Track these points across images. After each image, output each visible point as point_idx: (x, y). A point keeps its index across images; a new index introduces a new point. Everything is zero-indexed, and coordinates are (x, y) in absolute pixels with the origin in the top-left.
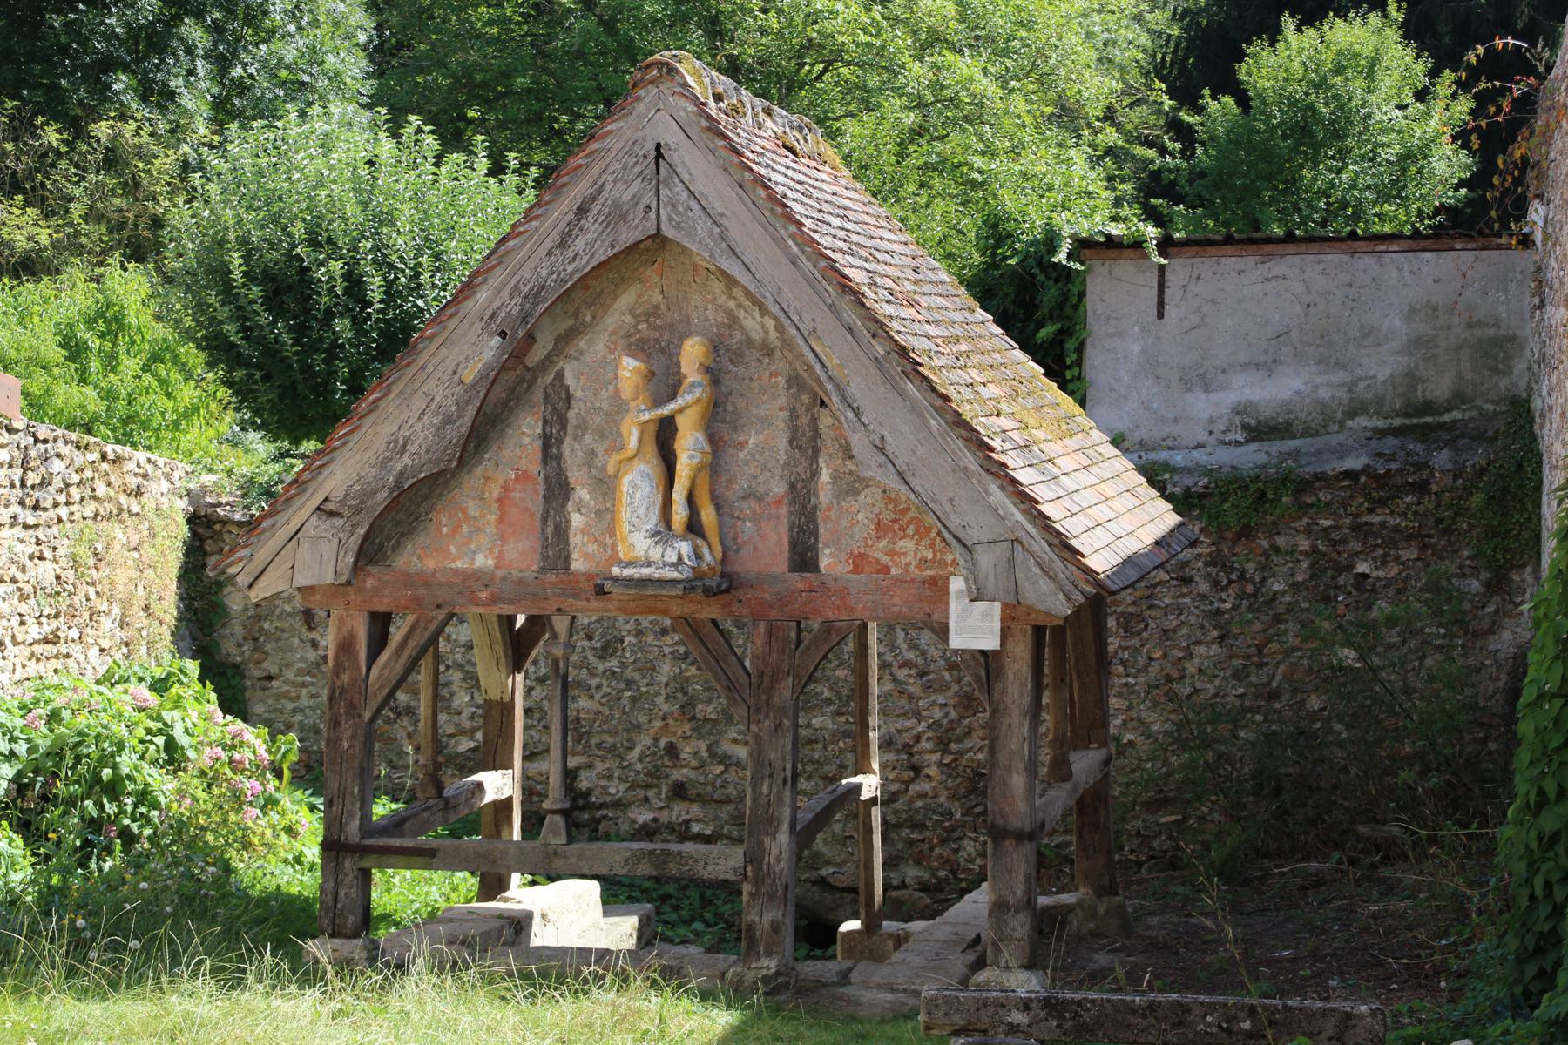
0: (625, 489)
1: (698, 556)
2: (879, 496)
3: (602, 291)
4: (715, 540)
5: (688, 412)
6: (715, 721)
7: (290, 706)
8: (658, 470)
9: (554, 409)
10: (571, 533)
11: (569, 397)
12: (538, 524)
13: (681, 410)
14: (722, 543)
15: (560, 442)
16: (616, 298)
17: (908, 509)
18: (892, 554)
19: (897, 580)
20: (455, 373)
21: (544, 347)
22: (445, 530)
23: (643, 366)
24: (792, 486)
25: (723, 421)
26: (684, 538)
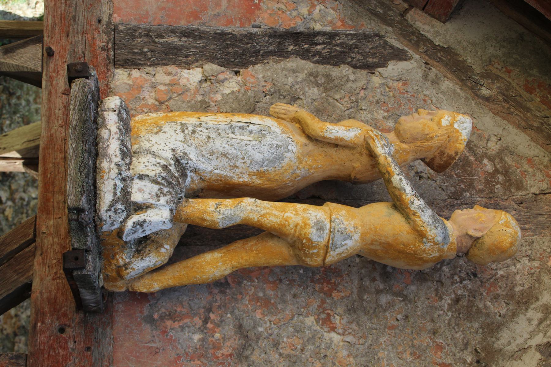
3: (528, 110)
5: (397, 219)
6: (12, 349)
7: (31, 99)
8: (288, 177)
10: (171, 69)
11: (371, 68)
12: (183, 24)
14: (167, 292)
15: (305, 55)
25: (362, 289)
26: (175, 218)
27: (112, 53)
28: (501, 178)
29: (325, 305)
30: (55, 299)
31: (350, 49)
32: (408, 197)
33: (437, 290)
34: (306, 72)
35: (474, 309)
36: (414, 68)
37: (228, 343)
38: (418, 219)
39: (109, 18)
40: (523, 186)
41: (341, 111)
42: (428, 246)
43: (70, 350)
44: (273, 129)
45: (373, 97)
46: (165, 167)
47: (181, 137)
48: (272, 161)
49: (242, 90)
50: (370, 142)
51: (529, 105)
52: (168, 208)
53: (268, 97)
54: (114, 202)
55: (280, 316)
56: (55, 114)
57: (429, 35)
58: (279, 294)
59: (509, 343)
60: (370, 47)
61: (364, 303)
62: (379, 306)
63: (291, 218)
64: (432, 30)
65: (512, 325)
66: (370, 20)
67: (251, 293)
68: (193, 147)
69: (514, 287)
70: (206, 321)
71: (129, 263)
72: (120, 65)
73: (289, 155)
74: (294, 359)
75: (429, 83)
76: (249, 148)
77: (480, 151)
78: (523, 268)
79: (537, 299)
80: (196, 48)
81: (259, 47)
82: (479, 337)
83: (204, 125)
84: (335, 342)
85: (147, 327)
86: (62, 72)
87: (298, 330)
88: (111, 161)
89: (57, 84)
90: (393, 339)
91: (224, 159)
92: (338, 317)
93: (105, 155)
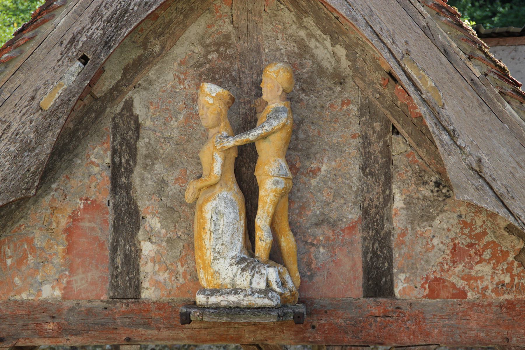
0: (208, 216)
1: (283, 284)
2: (455, 222)
3: (171, 22)
4: (294, 267)
5: (272, 138)
9: (124, 139)
10: (142, 262)
11: (138, 127)
12: (108, 253)
13: (265, 137)
15: (130, 171)
16: (185, 28)
17: (485, 233)
18: (468, 278)
19: (474, 305)
20: (33, 98)
21: (112, 77)
22: (9, 262)
23: (226, 92)
24: (366, 212)
27: (130, 300)
28: (222, 49)
29: (305, 172)
30: (295, 331)
31: (124, 139)
32: (263, 132)
33: (297, 102)
34: (143, 171)
35: (309, 80)
36: (140, 96)
37: (326, 232)
38: (276, 128)
39: (104, 302)
40: (227, 35)
41: (172, 150)
42: (289, 121)
43: (326, 322)
44: (214, 206)
45: (161, 127)
46: (243, 270)
47: (222, 260)
48: (233, 206)
49: (159, 215)
50: (225, 149)
51: (167, 19)
52: (268, 269)
53: (162, 199)
54: (268, 298)
55: (311, 201)
56: (173, 336)
57: (114, 83)
58: (297, 200)
59: (330, 62)
60: (122, 125)
61: (304, 148)
62: (306, 139)
63: (271, 199)
64: (109, 80)
65: (319, 59)
66: (102, 123)
67: (296, 217)
68: (229, 254)
69: (295, 53)
70: (312, 244)
71: (290, 290)
72: (139, 295)
73: (229, 196)
74: (336, 194)
75: (150, 87)
76: (228, 221)
77: (202, 60)
78: (282, 44)
79: (303, 39)
80: (125, 245)
81: (124, 202)
82: (326, 80)
83: (214, 247)
84: (327, 168)
85: (315, 279)
86: (143, 332)
87: (319, 190)
88: (243, 300)
89: (152, 335)
90: (326, 133)
91: (234, 236)
92: (312, 166)
93: (238, 303)
